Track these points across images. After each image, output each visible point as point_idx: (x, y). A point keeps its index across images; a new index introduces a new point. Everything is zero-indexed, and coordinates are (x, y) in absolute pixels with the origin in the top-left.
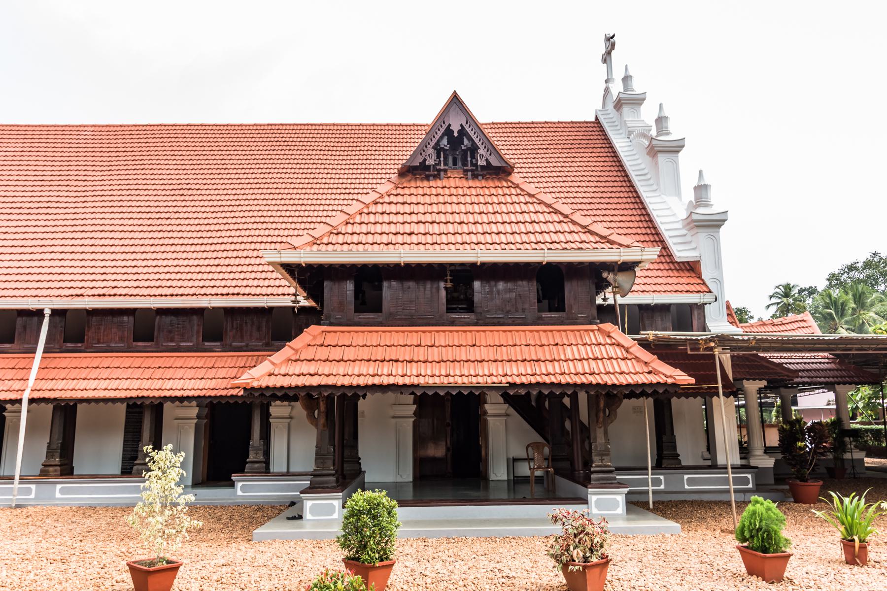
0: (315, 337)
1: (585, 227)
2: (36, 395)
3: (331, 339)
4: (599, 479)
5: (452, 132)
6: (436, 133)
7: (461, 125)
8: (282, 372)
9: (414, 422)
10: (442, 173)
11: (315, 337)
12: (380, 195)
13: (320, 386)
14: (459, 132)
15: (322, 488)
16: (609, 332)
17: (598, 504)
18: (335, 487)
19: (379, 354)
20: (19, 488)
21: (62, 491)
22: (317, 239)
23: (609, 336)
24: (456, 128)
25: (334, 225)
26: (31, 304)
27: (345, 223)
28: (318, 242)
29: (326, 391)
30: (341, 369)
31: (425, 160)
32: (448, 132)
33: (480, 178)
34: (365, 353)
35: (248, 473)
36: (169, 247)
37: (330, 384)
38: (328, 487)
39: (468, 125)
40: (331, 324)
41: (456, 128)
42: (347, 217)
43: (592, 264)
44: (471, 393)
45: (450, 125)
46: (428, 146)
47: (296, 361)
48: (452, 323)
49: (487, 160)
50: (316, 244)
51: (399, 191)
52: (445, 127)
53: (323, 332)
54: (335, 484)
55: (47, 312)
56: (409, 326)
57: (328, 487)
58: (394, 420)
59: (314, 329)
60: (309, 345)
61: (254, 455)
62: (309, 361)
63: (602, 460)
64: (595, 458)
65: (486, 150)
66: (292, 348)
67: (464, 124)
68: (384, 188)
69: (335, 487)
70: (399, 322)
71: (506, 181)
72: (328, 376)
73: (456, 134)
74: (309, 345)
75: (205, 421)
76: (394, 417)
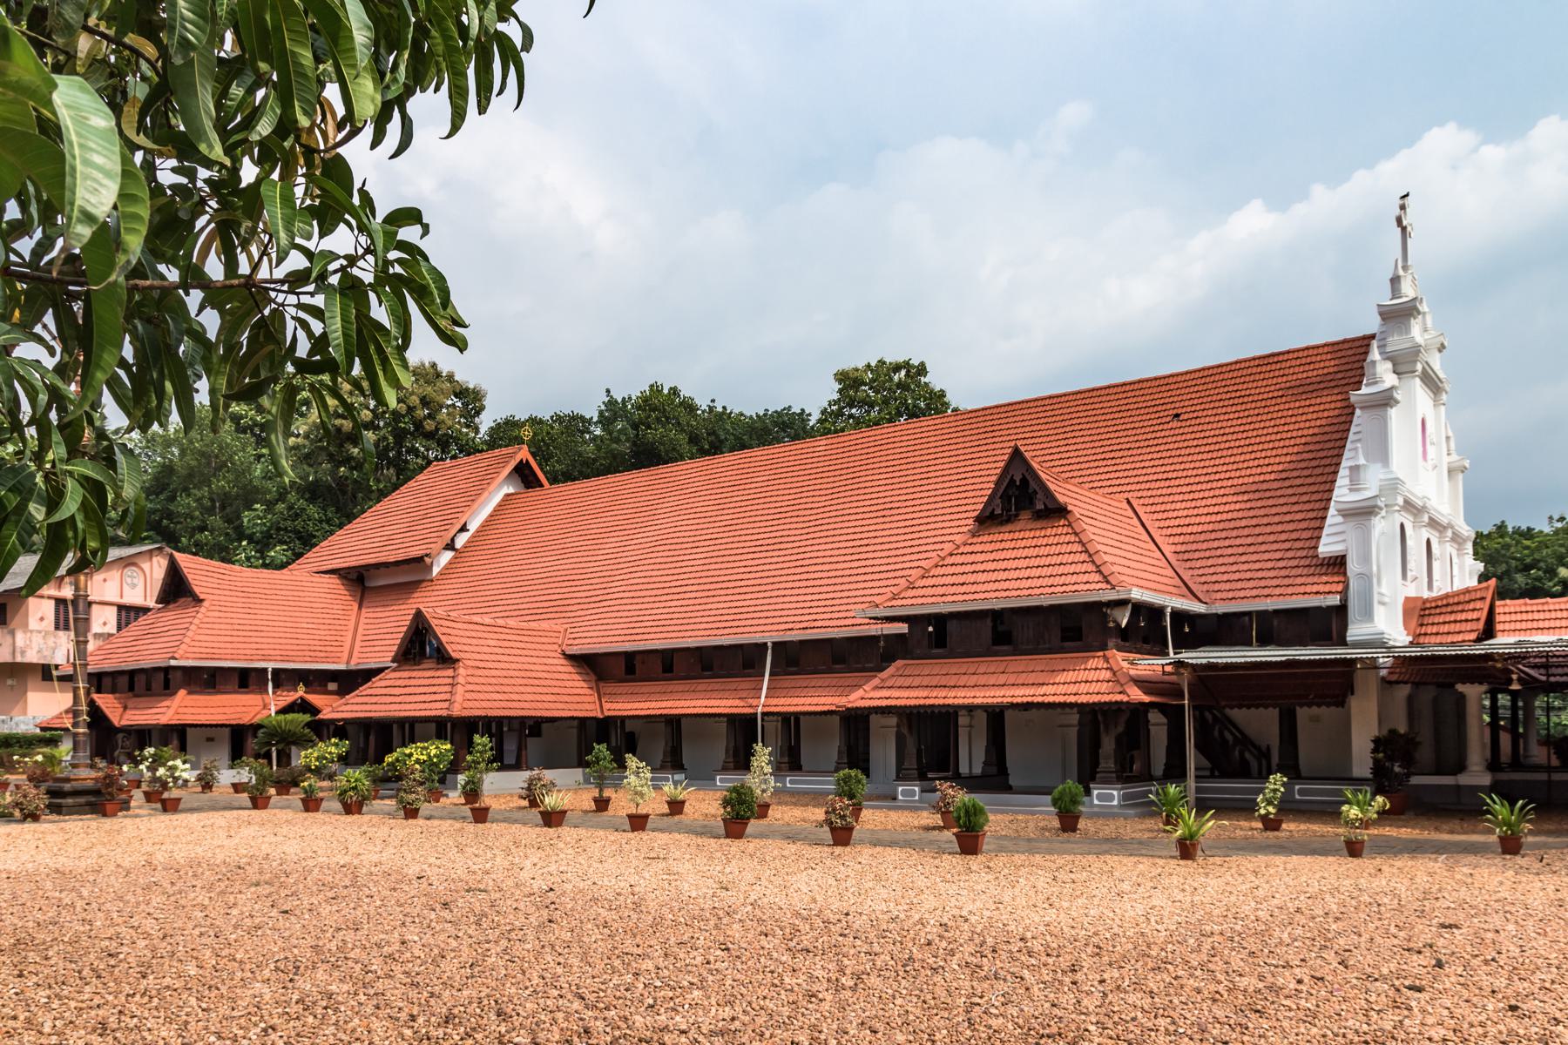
0: (898, 669)
1: (1098, 567)
2: (767, 709)
3: (238, 716)
17: (1099, 797)
20: (278, 765)
21: (791, 782)
24: (1018, 479)
26: (757, 638)
30: (905, 693)
41: (1018, 479)
44: (933, 712)
55: (769, 645)
59: (899, 663)
64: (1101, 761)
68: (959, 539)
71: (1066, 518)
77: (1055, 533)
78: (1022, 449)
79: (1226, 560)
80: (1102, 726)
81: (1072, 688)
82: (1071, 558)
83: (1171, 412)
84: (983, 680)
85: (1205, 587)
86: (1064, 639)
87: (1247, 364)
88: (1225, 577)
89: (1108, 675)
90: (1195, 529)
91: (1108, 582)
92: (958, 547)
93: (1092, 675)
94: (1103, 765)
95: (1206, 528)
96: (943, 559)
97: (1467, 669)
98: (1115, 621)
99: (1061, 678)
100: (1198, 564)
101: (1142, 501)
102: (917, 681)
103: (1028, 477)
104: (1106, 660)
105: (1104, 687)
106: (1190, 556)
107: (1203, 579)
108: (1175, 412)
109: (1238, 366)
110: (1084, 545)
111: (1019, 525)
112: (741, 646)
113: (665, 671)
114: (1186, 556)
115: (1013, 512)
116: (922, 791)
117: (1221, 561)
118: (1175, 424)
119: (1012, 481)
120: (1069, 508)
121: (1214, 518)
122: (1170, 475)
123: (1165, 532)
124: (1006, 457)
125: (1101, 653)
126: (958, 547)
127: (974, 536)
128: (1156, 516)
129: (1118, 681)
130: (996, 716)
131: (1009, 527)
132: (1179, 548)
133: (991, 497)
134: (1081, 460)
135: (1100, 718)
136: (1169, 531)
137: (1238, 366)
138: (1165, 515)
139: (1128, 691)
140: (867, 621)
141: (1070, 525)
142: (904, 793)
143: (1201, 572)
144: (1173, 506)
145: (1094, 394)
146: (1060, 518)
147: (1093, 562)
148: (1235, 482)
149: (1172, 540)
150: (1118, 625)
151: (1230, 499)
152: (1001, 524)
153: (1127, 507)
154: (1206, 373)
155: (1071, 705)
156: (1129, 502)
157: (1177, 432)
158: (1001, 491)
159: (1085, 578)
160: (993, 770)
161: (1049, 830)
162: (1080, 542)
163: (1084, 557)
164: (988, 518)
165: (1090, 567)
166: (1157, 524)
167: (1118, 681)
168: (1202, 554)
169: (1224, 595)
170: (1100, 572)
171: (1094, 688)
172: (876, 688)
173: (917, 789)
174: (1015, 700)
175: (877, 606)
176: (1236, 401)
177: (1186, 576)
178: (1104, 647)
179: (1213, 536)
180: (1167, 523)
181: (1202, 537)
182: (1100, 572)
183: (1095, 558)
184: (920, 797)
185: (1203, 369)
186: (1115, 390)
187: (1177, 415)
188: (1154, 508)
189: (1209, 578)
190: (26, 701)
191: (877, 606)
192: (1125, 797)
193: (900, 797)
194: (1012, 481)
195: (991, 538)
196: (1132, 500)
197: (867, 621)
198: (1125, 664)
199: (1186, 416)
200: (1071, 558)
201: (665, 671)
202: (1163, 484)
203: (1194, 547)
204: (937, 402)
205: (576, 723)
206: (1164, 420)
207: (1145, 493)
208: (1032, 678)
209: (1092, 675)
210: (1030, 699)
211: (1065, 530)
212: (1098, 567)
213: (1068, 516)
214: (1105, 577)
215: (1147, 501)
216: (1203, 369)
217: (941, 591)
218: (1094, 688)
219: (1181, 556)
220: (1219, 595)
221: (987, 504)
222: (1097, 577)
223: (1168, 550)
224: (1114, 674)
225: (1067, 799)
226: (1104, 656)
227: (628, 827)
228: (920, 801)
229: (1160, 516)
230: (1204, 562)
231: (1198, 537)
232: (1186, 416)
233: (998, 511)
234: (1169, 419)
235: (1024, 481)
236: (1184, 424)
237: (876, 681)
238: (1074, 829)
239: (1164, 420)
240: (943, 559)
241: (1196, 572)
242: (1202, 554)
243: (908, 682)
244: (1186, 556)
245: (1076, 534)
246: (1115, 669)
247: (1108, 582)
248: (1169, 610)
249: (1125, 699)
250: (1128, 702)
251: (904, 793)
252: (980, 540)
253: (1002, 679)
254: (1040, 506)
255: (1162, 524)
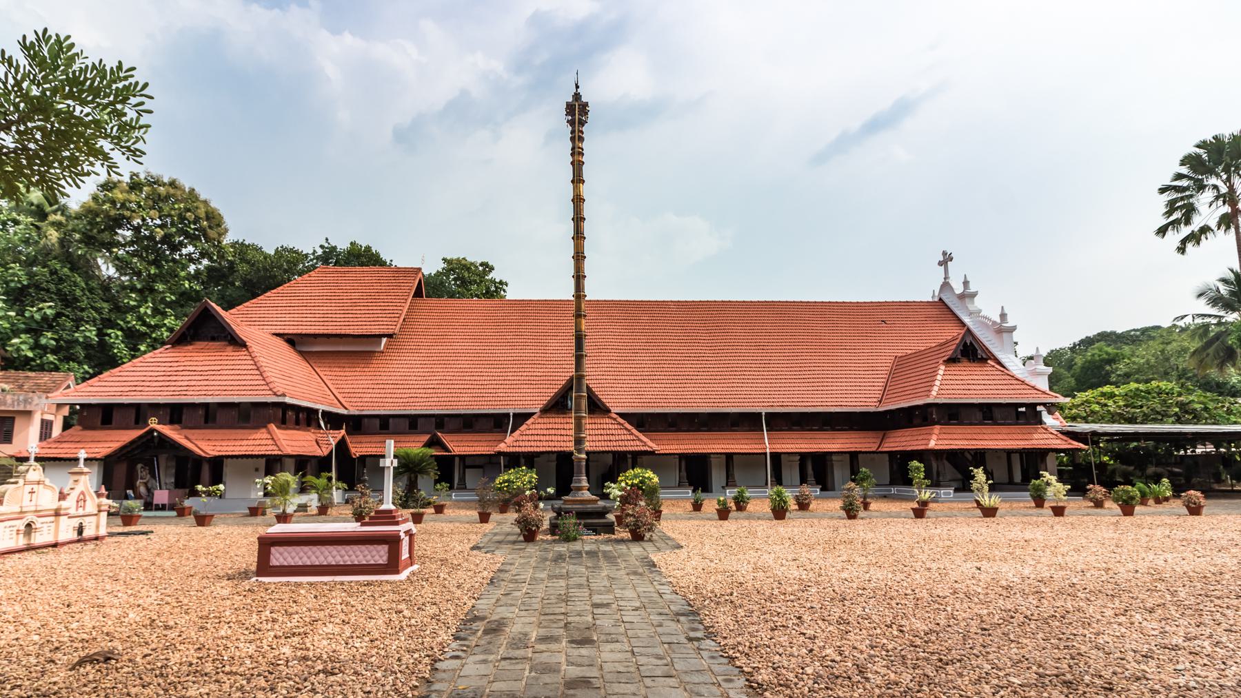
77: (990, 368)
81: (251, 448)
97: (1136, 436)
104: (269, 433)
112: (698, 414)
113: (381, 429)
130: (729, 457)
182: (262, 375)
183: (261, 369)
190: (28, 432)
194: (966, 343)
201: (381, 429)
204: (494, 291)
205: (555, 456)
227: (717, 517)
228: (953, 497)
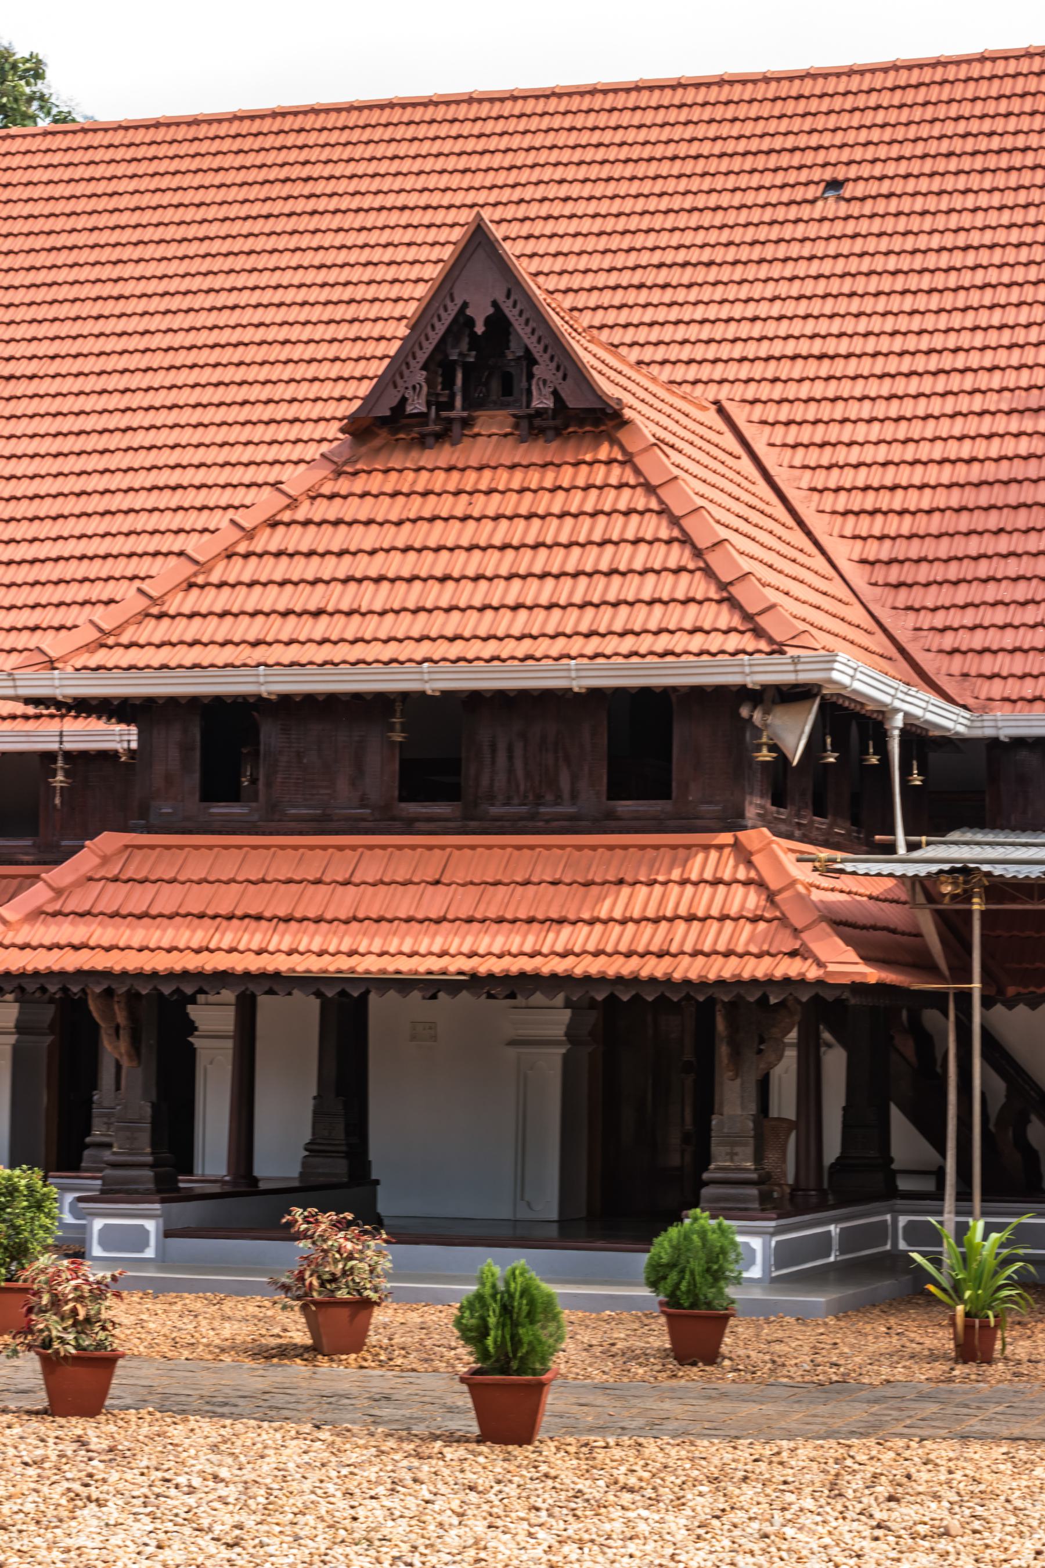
0: (105, 860)
1: (723, 586)
4: (718, 1199)
5: (470, 322)
6: (433, 328)
7: (495, 304)
8: (19, 941)
9: (566, 1058)
10: (456, 428)
11: (105, 860)
12: (287, 501)
13: (79, 973)
14: (488, 321)
15: (127, 1192)
16: (751, 854)
18: (147, 1192)
19: (226, 900)
22: (109, 634)
23: (749, 864)
25: (154, 594)
27: (184, 586)
28: (111, 641)
29: (99, 983)
30: (137, 934)
31: (404, 400)
32: (463, 322)
33: (550, 434)
34: (197, 899)
35: (87, 1170)
36: (379, 250)
37: (100, 968)
38: (136, 1192)
39: (510, 302)
40: (150, 830)
41: (480, 314)
42: (192, 568)
43: (721, 690)
45: (465, 305)
46: (412, 363)
47: (54, 914)
48: (409, 826)
49: (555, 393)
50: (105, 646)
51: (343, 485)
52: (453, 309)
53: (127, 847)
54: (151, 1186)
56: (315, 833)
57: (136, 1192)
58: (512, 1052)
59: (108, 841)
60: (90, 879)
61: (104, 1128)
62: (82, 915)
63: (732, 1155)
64: (716, 1149)
65: (554, 365)
66: (49, 886)
67: (501, 298)
68: (295, 479)
69: (147, 1192)
70: (292, 825)
71: (614, 441)
72: (108, 949)
73: (480, 329)
74: (90, 879)
75: (49, 1039)
76: (513, 1043)
78: (498, 232)
79: (1006, 591)
80: (723, 1051)
81: (649, 937)
82: (641, 557)
83: (817, 174)
84: (375, 903)
85: (957, 664)
86: (616, 791)
87: (1012, 67)
88: (1009, 639)
89: (753, 900)
90: (912, 500)
91: (758, 632)
92: (293, 503)
93: (705, 900)
94: (720, 1162)
95: (941, 498)
96: (250, 534)
98: (774, 748)
99: (610, 906)
100: (931, 597)
101: (758, 412)
102: (168, 899)
103: (511, 313)
104: (745, 857)
105: (744, 936)
106: (908, 573)
107: (948, 641)
108: (828, 174)
109: (988, 69)
110: (675, 521)
111: (478, 451)
114: (894, 574)
115: (458, 411)
116: (168, 1233)
117: (991, 592)
118: (831, 207)
119: (463, 322)
120: (628, 413)
121: (961, 473)
122: (831, 346)
123: (828, 501)
124: (447, 253)
125: (726, 838)
126: (293, 503)
127: (339, 474)
128: (799, 457)
129: (783, 920)
131: (445, 455)
132: (872, 550)
133: (399, 364)
134: (198, 302)
135: (721, 1025)
136: (842, 502)
137: (988, 69)
138: (826, 456)
139: (817, 948)
140: (20, 708)
141: (628, 460)
142: (108, 1238)
143: (939, 620)
144: (847, 433)
145: (160, 134)
146: (598, 438)
147: (708, 572)
148: (1011, 379)
149: (850, 525)
150: (783, 759)
151: (1001, 424)
152: (422, 442)
153: (720, 424)
154: (903, 78)
155: (556, 983)
156: (721, 411)
157: (838, 228)
158: (429, 347)
159: (690, 616)
160: (339, 1168)
161: (641, 1357)
162: (664, 511)
163: (677, 556)
164: (383, 421)
165: (701, 587)
166: (806, 479)
167: (783, 920)
168: (938, 572)
169: (1013, 689)
170: (732, 602)
171: (714, 937)
172: (38, 914)
173: (150, 1225)
174: (484, 967)
175: (51, 664)
176: (992, 162)
177: (902, 626)
178: (733, 822)
179: (964, 522)
180: (834, 479)
181: (935, 524)
182: (732, 602)
184: (160, 1249)
185: (895, 67)
186: (655, 98)
187: (835, 185)
188: (792, 435)
189: (964, 640)
191: (51, 664)
192: (783, 1256)
193: (97, 1251)
195: (391, 483)
196: (730, 407)
197: (20, 708)
198: (803, 873)
199: (860, 189)
200: (641, 557)
202: (812, 368)
203: (915, 550)
206: (799, 194)
207: (765, 391)
208: (523, 901)
209: (705, 900)
210: (528, 965)
211: (616, 475)
212: (723, 586)
213: (622, 435)
214: (747, 617)
215: (771, 413)
216: (896, 67)
217: (254, 629)
218: (714, 937)
219: (880, 574)
220: (997, 689)
221: (385, 383)
222: (725, 618)
223: (843, 552)
224: (771, 898)
225: (697, 1265)
226: (737, 845)
228: (162, 1260)
229: (813, 457)
230: (945, 595)
231: (922, 525)
232: (860, 189)
233: (417, 405)
234: (811, 192)
235: (498, 322)
236: (855, 209)
237: (37, 895)
238: (711, 1356)
239: (799, 194)
240: (250, 534)
241: (926, 620)
242: (938, 572)
243: (139, 899)
244: (894, 574)
245: (650, 489)
246: (774, 885)
247: (758, 632)
248: (899, 721)
249: (813, 973)
250: (820, 983)
251: (108, 1238)
252: (359, 485)
253: (434, 903)
254: (543, 401)
255: (820, 479)
